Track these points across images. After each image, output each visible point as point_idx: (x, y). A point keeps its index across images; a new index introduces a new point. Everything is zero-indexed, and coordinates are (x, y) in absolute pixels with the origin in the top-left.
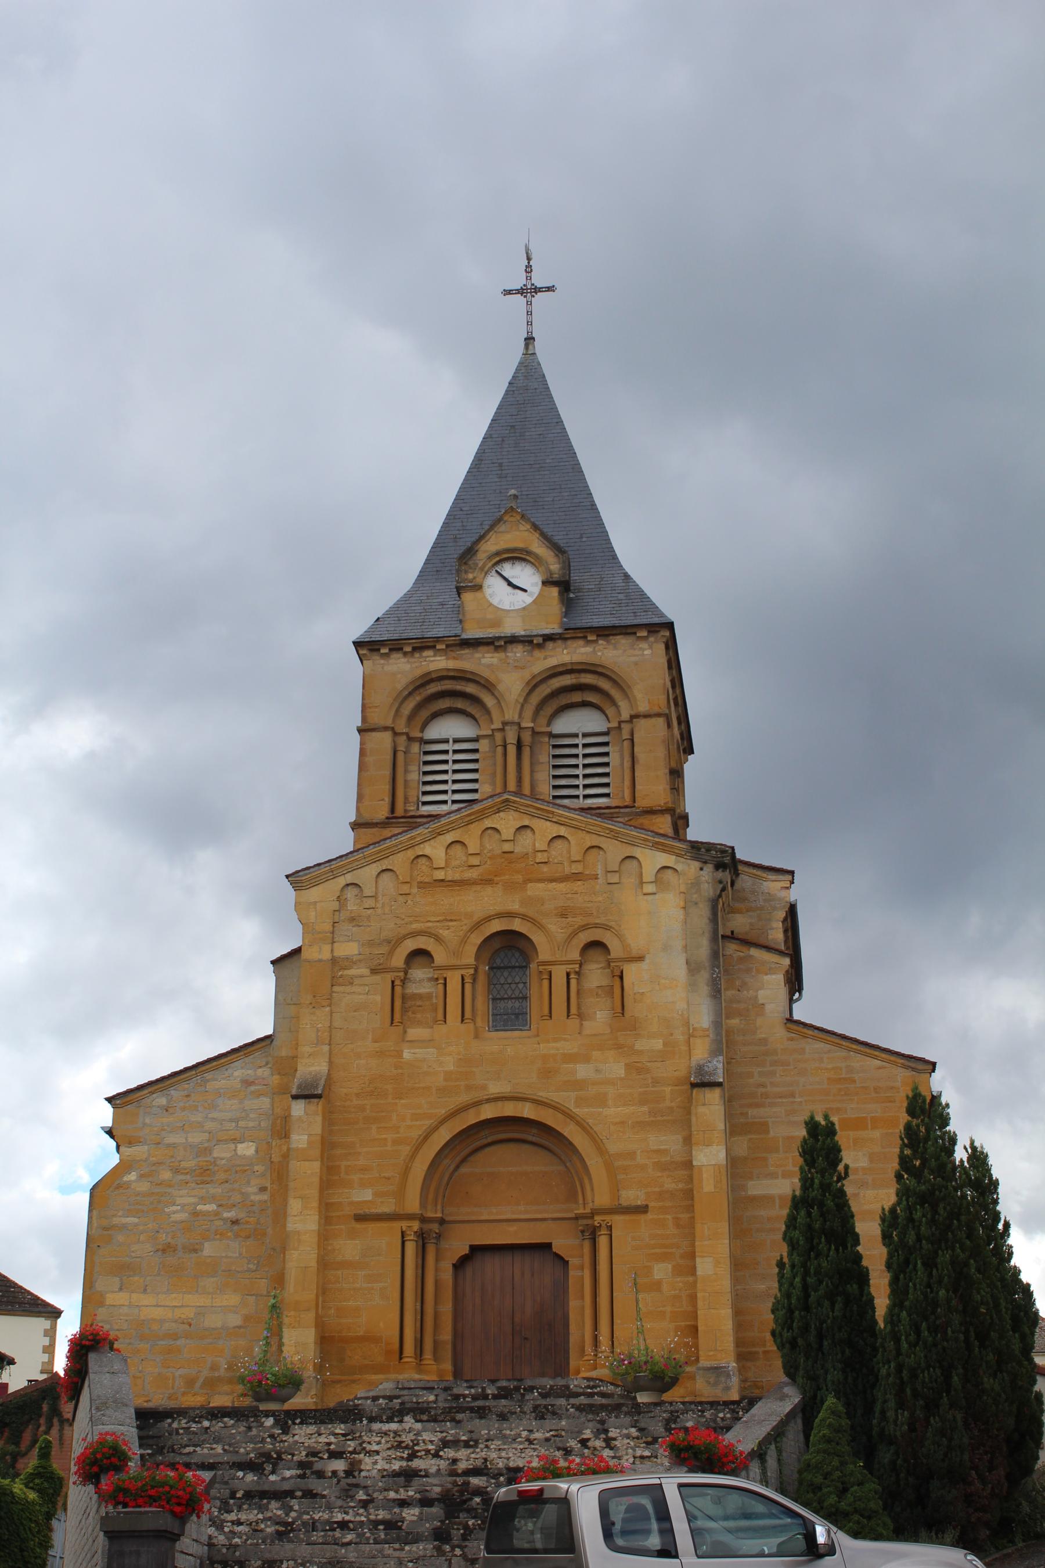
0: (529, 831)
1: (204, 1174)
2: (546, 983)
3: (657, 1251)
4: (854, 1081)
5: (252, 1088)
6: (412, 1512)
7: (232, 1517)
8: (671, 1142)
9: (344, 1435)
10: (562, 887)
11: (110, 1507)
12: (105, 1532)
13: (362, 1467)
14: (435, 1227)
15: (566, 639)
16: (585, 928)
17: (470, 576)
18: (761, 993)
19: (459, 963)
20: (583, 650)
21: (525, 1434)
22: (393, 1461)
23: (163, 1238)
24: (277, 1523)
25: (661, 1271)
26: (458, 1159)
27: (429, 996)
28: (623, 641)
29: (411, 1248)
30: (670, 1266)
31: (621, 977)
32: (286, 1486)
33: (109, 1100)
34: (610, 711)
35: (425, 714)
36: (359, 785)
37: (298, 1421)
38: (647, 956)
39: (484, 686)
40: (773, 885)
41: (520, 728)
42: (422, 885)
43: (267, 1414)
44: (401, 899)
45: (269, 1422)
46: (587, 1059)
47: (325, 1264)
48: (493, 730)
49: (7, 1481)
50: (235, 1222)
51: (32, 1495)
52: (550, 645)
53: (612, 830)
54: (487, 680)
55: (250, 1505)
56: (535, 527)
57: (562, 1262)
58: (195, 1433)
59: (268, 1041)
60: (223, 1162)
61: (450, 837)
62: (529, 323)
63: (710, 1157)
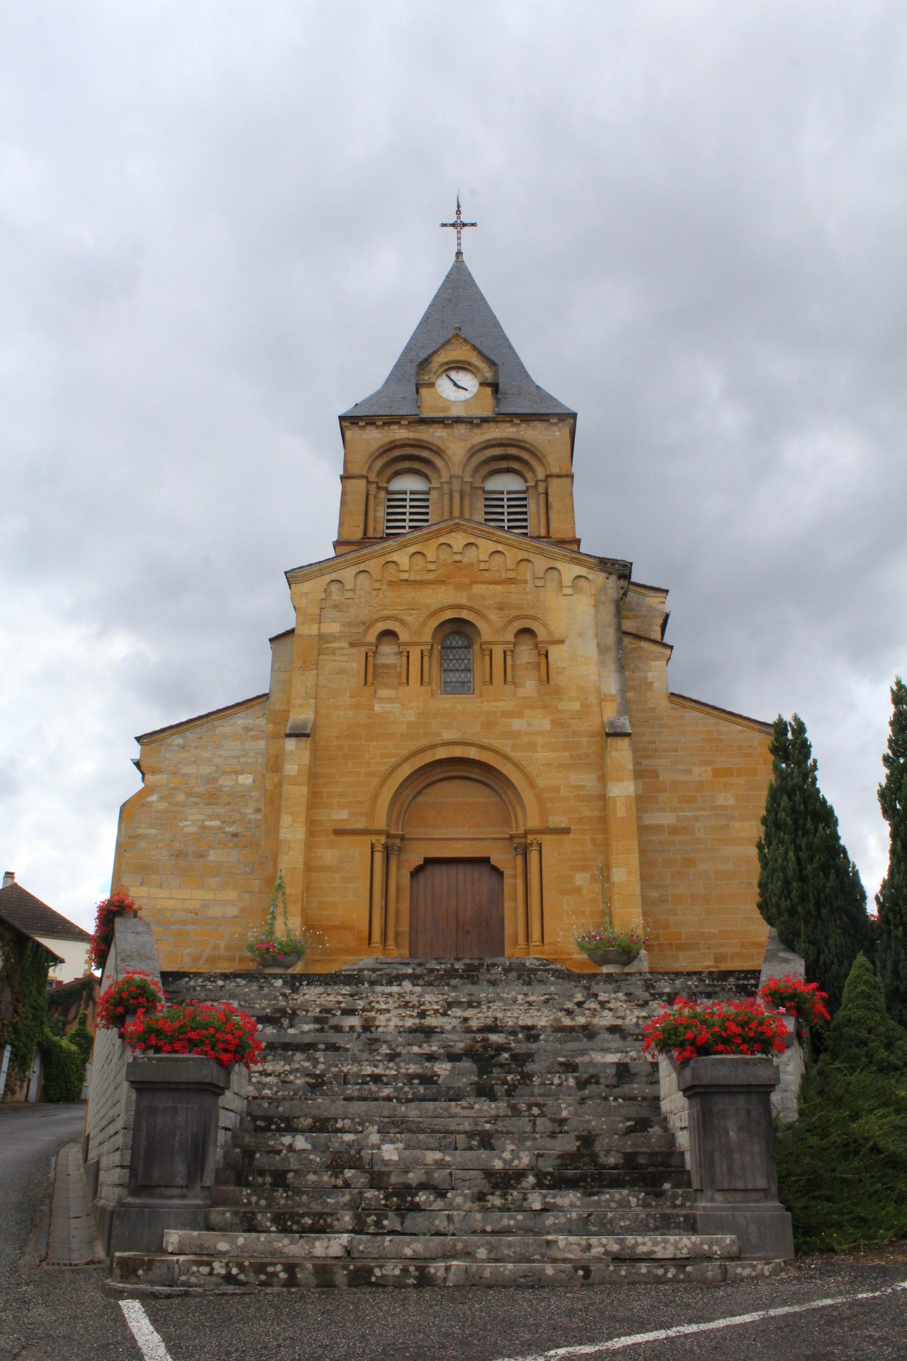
0: (474, 548)
1: (211, 798)
2: (487, 658)
3: (577, 863)
4: (723, 741)
5: (252, 733)
6: (444, 1066)
7: (259, 1067)
8: (588, 780)
9: (351, 995)
10: (499, 588)
11: (138, 1053)
12: (133, 1083)
13: (377, 1023)
14: (397, 842)
15: (497, 422)
16: (518, 618)
17: (426, 378)
18: (650, 674)
19: (420, 640)
20: (510, 430)
21: (520, 997)
22: (406, 1018)
23: (177, 845)
24: (308, 1075)
25: (581, 879)
26: (425, 783)
27: (394, 666)
28: (540, 425)
29: (379, 857)
30: (588, 875)
31: (547, 656)
32: (307, 1039)
33: (138, 739)
34: (529, 476)
35: (389, 471)
36: (341, 515)
37: (305, 983)
38: (567, 641)
39: (436, 452)
40: (653, 600)
41: (463, 482)
42: (391, 583)
43: (276, 976)
44: (374, 593)
45: (279, 983)
46: (520, 715)
47: (309, 867)
48: (442, 483)
49: (57, 1038)
50: (235, 835)
51: (74, 1048)
52: (485, 425)
53: (538, 548)
54: (438, 447)
55: (274, 1056)
56: (474, 348)
57: (498, 872)
58: (210, 990)
59: (265, 698)
60: (227, 789)
61: (413, 549)
62: (459, 244)
63: (623, 790)
